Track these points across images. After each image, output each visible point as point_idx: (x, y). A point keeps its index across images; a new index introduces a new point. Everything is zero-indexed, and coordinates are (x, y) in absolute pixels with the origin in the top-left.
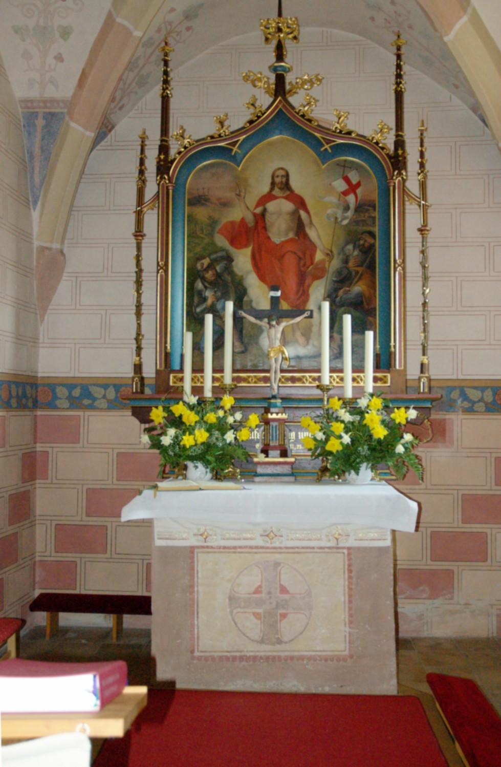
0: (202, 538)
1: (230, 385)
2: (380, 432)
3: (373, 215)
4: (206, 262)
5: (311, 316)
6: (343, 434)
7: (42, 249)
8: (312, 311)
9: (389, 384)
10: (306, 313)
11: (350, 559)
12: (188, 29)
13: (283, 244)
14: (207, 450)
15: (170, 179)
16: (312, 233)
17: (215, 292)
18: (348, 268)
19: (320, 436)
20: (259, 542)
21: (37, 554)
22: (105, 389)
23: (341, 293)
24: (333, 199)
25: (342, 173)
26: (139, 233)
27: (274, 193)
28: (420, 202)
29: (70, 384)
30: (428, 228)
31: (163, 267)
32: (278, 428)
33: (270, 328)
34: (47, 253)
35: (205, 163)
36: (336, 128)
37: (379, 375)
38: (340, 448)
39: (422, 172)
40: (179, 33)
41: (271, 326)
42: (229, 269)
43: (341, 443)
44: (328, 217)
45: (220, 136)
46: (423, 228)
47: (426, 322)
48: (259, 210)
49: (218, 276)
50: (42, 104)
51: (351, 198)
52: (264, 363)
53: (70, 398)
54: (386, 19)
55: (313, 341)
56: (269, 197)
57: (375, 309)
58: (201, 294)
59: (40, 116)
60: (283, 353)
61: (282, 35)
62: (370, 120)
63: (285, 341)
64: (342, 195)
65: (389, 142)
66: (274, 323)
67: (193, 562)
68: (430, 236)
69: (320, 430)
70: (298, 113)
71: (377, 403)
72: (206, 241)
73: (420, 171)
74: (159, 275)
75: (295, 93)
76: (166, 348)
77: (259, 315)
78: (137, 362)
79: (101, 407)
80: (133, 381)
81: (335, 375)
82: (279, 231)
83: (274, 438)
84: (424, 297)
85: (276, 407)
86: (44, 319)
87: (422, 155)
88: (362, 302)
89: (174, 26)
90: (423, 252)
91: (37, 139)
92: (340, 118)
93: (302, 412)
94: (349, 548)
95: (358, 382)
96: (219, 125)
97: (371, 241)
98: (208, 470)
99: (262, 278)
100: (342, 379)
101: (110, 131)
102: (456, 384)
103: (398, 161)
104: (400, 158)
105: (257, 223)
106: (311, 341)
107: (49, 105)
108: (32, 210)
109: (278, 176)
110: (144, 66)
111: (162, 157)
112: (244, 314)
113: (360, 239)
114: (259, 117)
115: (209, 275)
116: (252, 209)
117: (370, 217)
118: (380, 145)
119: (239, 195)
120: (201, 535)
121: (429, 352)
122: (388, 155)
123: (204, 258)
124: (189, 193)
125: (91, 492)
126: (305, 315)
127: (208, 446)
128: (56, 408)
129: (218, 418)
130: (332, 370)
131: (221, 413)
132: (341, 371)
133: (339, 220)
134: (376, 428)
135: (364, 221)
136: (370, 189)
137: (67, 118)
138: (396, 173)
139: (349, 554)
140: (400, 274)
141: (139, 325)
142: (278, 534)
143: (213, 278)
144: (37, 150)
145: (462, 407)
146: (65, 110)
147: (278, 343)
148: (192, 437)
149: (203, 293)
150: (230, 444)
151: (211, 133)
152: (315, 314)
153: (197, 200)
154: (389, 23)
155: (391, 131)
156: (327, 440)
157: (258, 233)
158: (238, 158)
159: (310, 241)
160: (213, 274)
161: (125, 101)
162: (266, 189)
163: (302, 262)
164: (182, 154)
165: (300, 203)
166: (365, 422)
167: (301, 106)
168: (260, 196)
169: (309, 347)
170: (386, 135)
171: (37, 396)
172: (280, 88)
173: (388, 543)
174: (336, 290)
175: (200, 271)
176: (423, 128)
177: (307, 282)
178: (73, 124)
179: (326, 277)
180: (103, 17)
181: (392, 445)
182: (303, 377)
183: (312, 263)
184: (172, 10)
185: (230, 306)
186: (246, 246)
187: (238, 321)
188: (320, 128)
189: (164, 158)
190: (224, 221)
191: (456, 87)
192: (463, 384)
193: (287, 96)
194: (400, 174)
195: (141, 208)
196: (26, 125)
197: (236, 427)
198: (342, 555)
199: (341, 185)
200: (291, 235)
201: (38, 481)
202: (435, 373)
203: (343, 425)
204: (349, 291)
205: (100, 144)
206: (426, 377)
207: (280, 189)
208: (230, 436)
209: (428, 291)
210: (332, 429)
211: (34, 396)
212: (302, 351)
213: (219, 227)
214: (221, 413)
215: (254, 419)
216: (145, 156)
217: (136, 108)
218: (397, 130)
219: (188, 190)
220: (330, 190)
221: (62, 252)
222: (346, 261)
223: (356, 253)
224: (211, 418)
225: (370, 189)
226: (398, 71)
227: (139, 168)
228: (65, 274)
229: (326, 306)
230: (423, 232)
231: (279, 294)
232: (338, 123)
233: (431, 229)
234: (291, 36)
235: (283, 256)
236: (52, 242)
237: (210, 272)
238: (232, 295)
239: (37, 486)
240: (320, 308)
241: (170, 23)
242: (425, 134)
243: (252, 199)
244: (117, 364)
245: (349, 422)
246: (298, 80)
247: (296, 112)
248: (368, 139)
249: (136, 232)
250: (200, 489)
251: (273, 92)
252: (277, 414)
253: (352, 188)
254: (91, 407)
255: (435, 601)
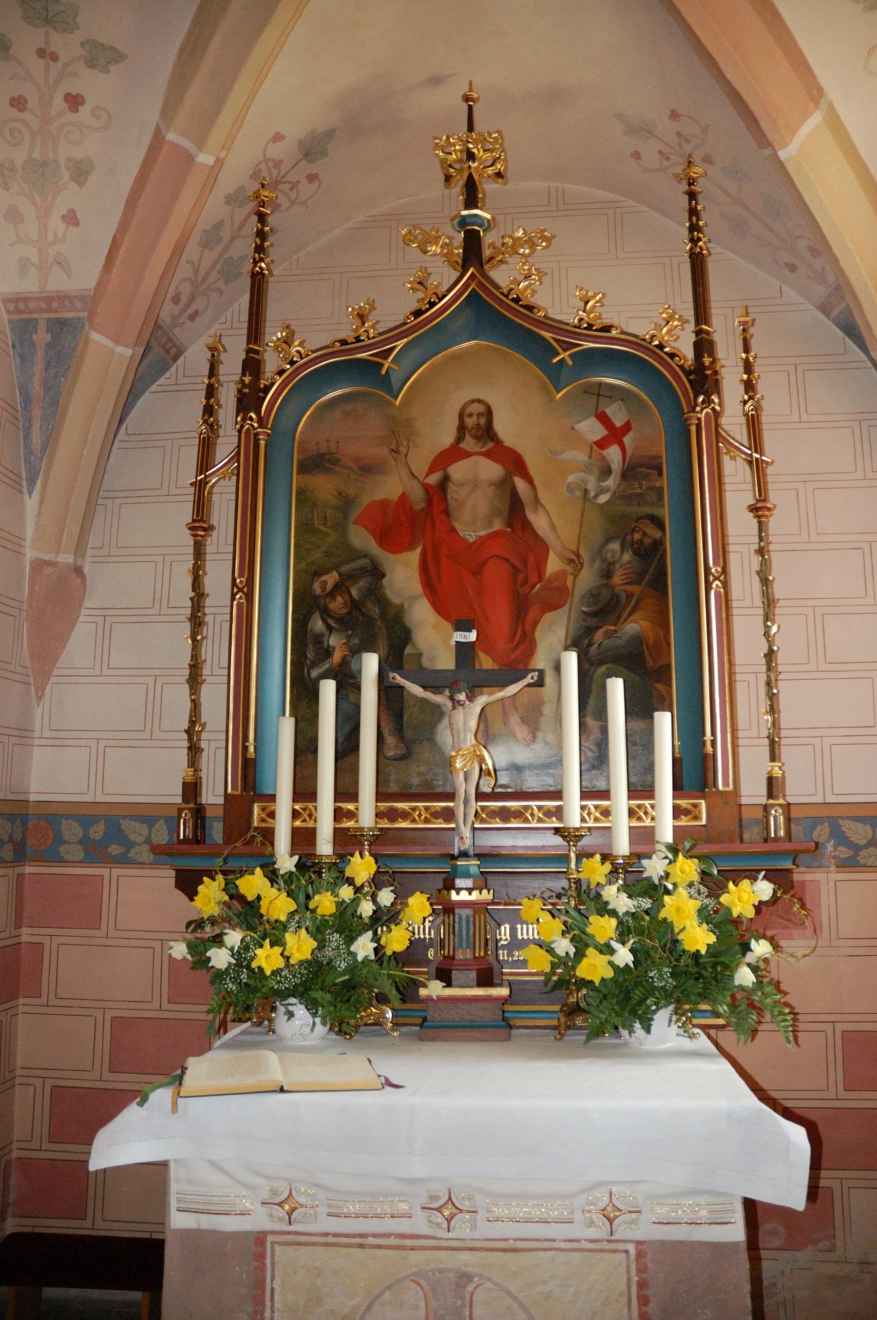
0: (281, 1213)
1: (370, 829)
2: (698, 938)
3: (658, 484)
4: (331, 579)
5: (540, 683)
6: (615, 945)
7: (38, 565)
8: (541, 672)
9: (704, 823)
10: (530, 676)
11: (642, 1269)
12: (311, 178)
13: (482, 541)
14: (316, 975)
15: (262, 422)
16: (539, 521)
17: (349, 638)
18: (612, 589)
19: (564, 946)
20: (420, 1224)
21: (15, 1145)
22: (150, 827)
23: (599, 636)
24: (581, 456)
25: (594, 407)
26: (200, 525)
27: (463, 445)
28: (751, 456)
29: (85, 815)
30: (769, 505)
31: (243, 588)
32: (472, 919)
33: (454, 708)
34: (48, 570)
35: (331, 395)
36: (581, 320)
37: (683, 803)
38: (609, 973)
39: (750, 398)
40: (294, 186)
41: (456, 704)
42: (375, 592)
43: (611, 963)
44: (570, 489)
45: (358, 339)
46: (759, 505)
47: (775, 691)
48: (434, 479)
49: (355, 605)
50: (43, 305)
51: (613, 454)
52: (446, 780)
53: (85, 842)
54: (660, 152)
55: (546, 734)
56: (454, 454)
57: (669, 666)
58: (321, 643)
59: (42, 326)
60: (482, 760)
61: (474, 165)
62: (644, 304)
63: (486, 733)
64: (595, 448)
65: (686, 347)
66: (462, 697)
67: (262, 1268)
68: (774, 524)
69: (563, 933)
70: (507, 296)
71: (688, 869)
72: (331, 539)
73: (746, 397)
74: (235, 603)
75: (501, 262)
76: (245, 749)
77: (433, 682)
78: (190, 779)
79: (141, 861)
80: (180, 817)
81: (590, 803)
82: (474, 517)
83: (464, 943)
84: (768, 641)
85: (467, 875)
86: (43, 694)
87: (748, 368)
88: (641, 654)
89: (284, 168)
90: (761, 552)
91: (38, 368)
92: (587, 303)
93: (523, 882)
94: (638, 1243)
95: (639, 819)
96: (358, 321)
97: (654, 533)
98: (318, 1020)
99: (440, 608)
100: (606, 813)
101: (175, 359)
102: (824, 812)
103: (703, 379)
104: (708, 372)
105: (429, 502)
106: (540, 735)
107: (55, 305)
108: (26, 496)
109: (471, 415)
110: (233, 240)
111: (247, 379)
112: (399, 680)
113: (633, 531)
114: (432, 304)
115: (337, 605)
116: (421, 479)
117: (653, 489)
118: (667, 350)
119: (397, 452)
120: (280, 1204)
121: (785, 752)
122: (681, 367)
123: (328, 571)
124: (302, 450)
125: (121, 1026)
126: (528, 680)
127: (316, 969)
128: (62, 861)
129: (340, 904)
130: (585, 795)
131: (346, 893)
132: (605, 794)
133: (592, 494)
134: (688, 928)
135: (641, 495)
136: (650, 435)
137: (86, 328)
138: (701, 399)
139: (640, 1255)
140: (717, 594)
141: (196, 705)
142: (466, 1205)
143: (344, 611)
144: (36, 388)
145: (835, 857)
146: (85, 314)
147: (470, 740)
148: (278, 950)
149: (325, 639)
150: (366, 961)
151: (342, 335)
152: (549, 679)
153: (316, 463)
154: (668, 159)
155: (686, 326)
156: (580, 954)
157: (433, 522)
158: (395, 380)
159: (536, 535)
160: (345, 603)
161: (199, 304)
162: (446, 437)
163: (521, 577)
164: (287, 373)
165: (515, 463)
166: (663, 914)
167: (512, 282)
168: (439, 451)
169: (538, 747)
170: (677, 332)
171: (24, 838)
172: (472, 252)
173: (737, 1232)
174: (589, 631)
175: (320, 596)
176: (747, 319)
177: (530, 617)
178: (95, 336)
179: (568, 605)
180: (147, 139)
181: (727, 967)
182: (526, 808)
183: (540, 578)
184: (278, 137)
185: (370, 663)
186: (411, 547)
187: (389, 695)
188: (548, 324)
189: (250, 381)
190: (366, 500)
191: (792, 268)
192: (835, 813)
193: (486, 267)
194: (708, 401)
195: (206, 477)
196: (17, 343)
197: (384, 918)
198: (624, 1255)
199: (592, 429)
200: (498, 525)
201: (21, 1001)
202: (797, 791)
203: (614, 922)
204: (615, 632)
205: (158, 383)
206: (780, 805)
207: (475, 437)
208: (363, 947)
209: (774, 629)
210: (589, 930)
211: (18, 837)
212: (522, 754)
213: (354, 514)
214: (346, 893)
215: (418, 905)
216: (218, 382)
217: (223, 319)
218: (698, 322)
219: (300, 443)
220: (573, 438)
221: (78, 571)
222: (607, 574)
223: (627, 557)
224: (325, 904)
225: (650, 435)
226: (694, 219)
227: (204, 402)
228: (84, 612)
229: (571, 660)
230: (760, 513)
231: (472, 636)
232: (584, 311)
233: (775, 506)
234: (490, 171)
235: (484, 564)
236: (58, 552)
237: (339, 599)
238: (383, 643)
239: (21, 1009)
240: (557, 668)
241: (277, 164)
242: (752, 330)
243: (420, 460)
244: (153, 778)
245: (627, 913)
246: (506, 240)
247: (503, 294)
248: (644, 340)
249: (194, 521)
250: (282, 1090)
251: (460, 261)
252: (470, 891)
253: (615, 435)
254: (124, 861)
255: (798, 1254)
